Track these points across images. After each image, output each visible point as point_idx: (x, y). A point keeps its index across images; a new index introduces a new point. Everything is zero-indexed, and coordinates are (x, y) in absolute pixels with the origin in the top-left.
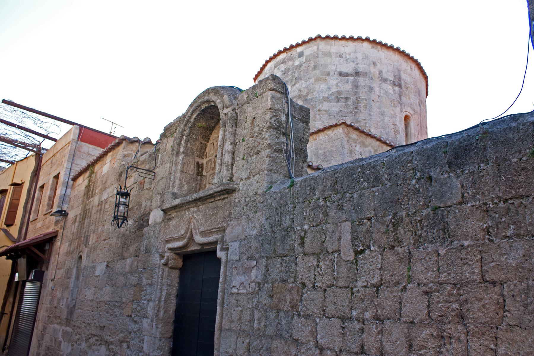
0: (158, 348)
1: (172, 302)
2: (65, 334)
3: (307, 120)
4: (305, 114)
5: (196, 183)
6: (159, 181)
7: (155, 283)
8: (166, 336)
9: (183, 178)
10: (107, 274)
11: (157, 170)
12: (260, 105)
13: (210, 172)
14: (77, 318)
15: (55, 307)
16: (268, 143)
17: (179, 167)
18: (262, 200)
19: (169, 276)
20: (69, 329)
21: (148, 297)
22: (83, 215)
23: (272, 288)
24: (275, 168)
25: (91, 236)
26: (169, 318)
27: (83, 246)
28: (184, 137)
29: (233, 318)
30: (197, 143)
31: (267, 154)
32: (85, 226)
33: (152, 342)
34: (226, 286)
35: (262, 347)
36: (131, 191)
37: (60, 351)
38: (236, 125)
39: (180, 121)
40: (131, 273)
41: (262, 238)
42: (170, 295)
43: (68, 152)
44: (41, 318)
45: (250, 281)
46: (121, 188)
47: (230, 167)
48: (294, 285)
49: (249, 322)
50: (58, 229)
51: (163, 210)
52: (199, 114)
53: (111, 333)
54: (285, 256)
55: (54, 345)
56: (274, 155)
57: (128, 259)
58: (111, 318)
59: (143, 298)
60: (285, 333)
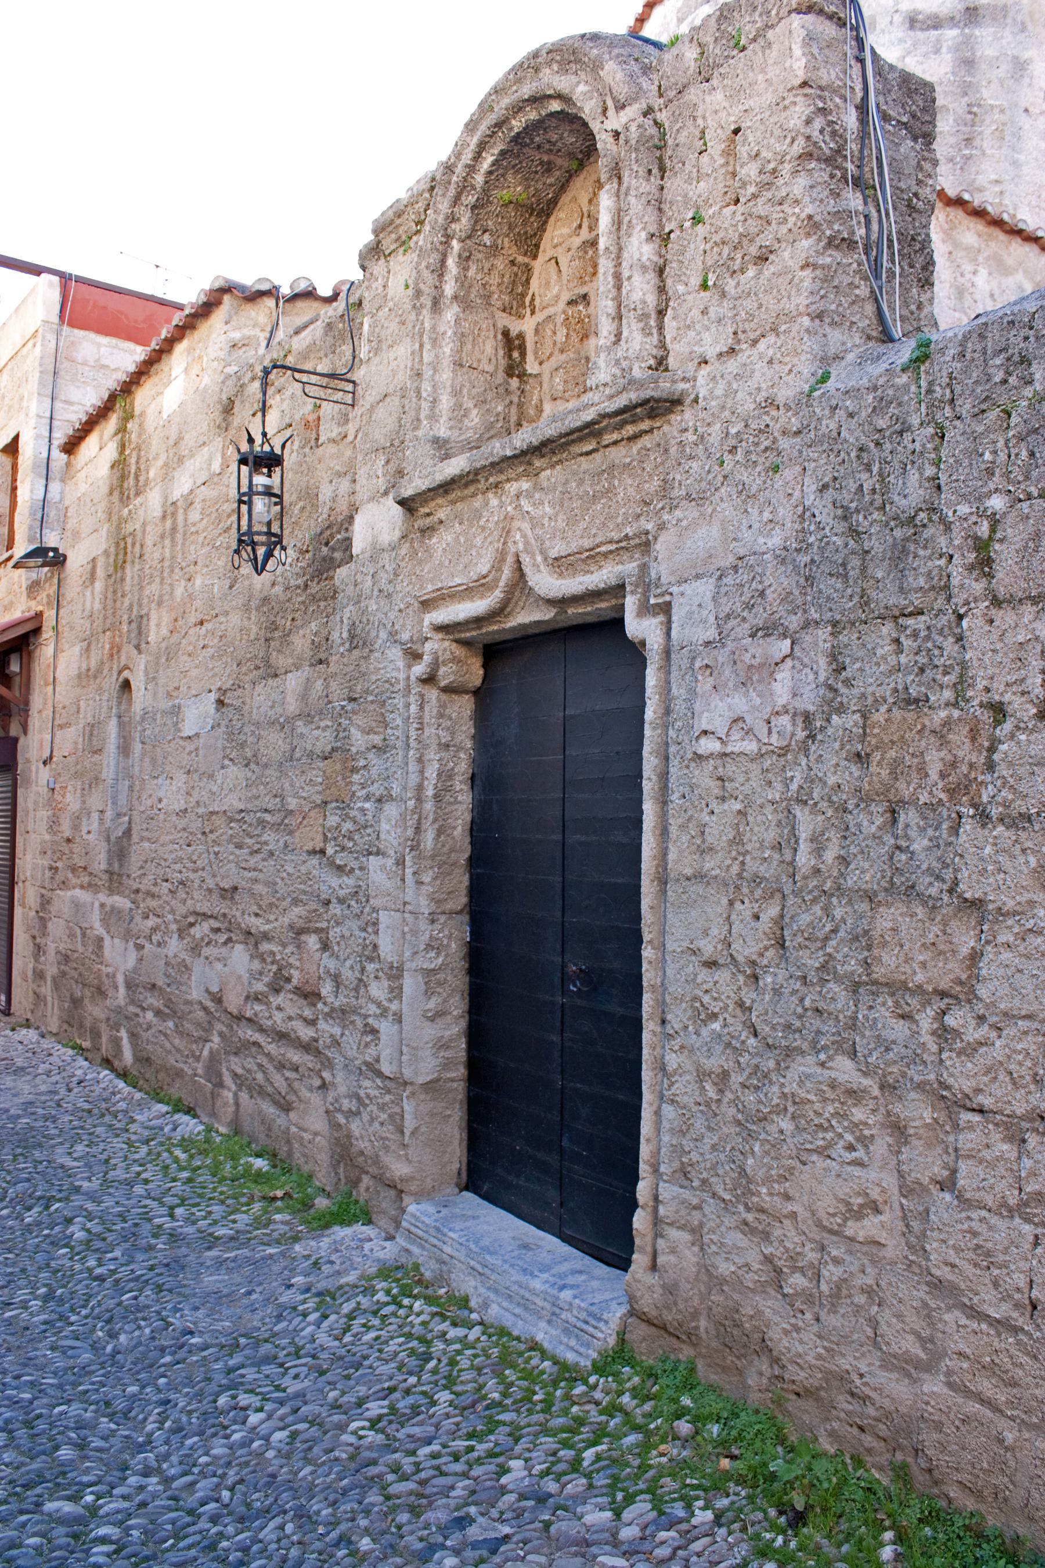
0: (429, 947)
1: (459, 798)
2: (110, 915)
3: (926, 128)
4: (921, 103)
5: (507, 401)
6: (372, 409)
7: (399, 744)
8: (449, 906)
9: (462, 386)
10: (223, 729)
11: (358, 375)
12: (760, 77)
13: (553, 360)
14: (142, 867)
15: (68, 840)
16: (803, 216)
17: (447, 350)
18: (795, 424)
19: (441, 716)
20: (121, 902)
21: (377, 789)
22: (117, 554)
23: (864, 727)
24: (833, 307)
25: (154, 615)
26: (452, 850)
27: (128, 651)
28: (455, 243)
29: (709, 839)
30: (500, 263)
31: (804, 255)
32: (127, 588)
33: (406, 929)
34: (672, 733)
35: (834, 931)
36: (283, 446)
37: (101, 963)
38: (662, 170)
39: (432, 188)
40: (307, 716)
41: (807, 559)
42: (450, 777)
43: (37, 363)
44: (28, 874)
45: (769, 709)
46: (251, 440)
47: (653, 323)
48: (956, 713)
49: (778, 847)
50: (40, 608)
51: (402, 503)
52: (503, 153)
53: (260, 907)
54: (911, 615)
55: (81, 949)
56: (828, 260)
57: (290, 675)
58: (253, 862)
59: (359, 794)
60: (928, 880)
